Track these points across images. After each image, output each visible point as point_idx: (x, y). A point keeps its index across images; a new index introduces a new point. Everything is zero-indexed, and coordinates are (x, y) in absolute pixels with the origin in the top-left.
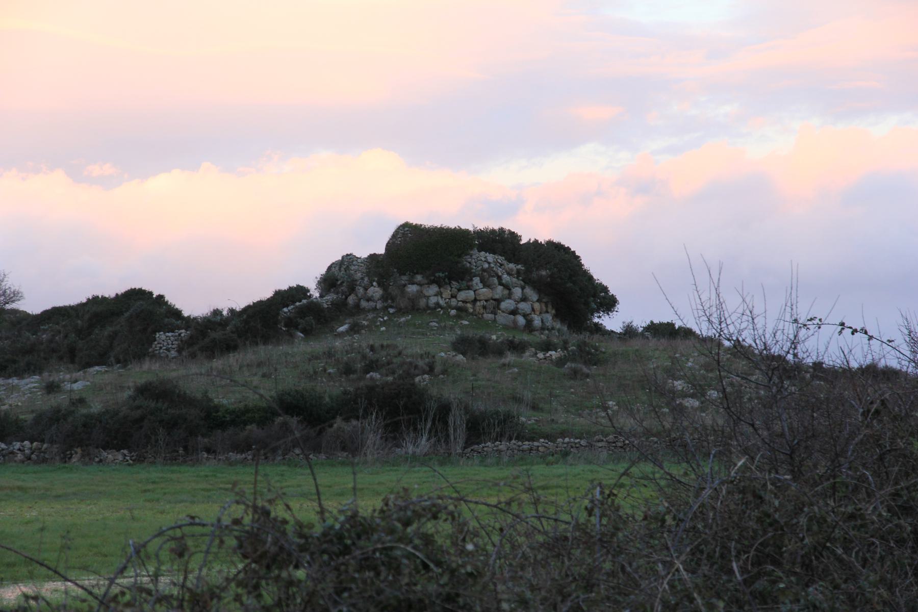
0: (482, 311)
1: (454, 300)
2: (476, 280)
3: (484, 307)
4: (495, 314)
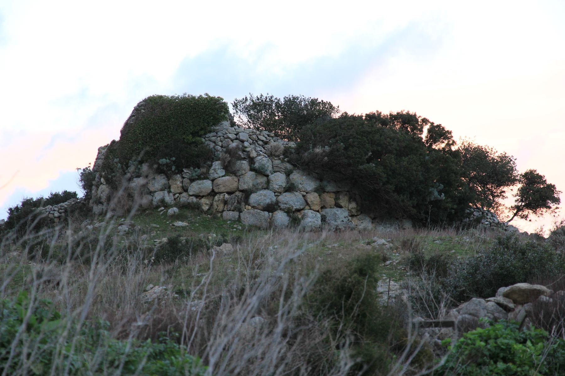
0: (221, 207)
1: (184, 194)
2: (217, 165)
3: (225, 202)
4: (240, 211)
